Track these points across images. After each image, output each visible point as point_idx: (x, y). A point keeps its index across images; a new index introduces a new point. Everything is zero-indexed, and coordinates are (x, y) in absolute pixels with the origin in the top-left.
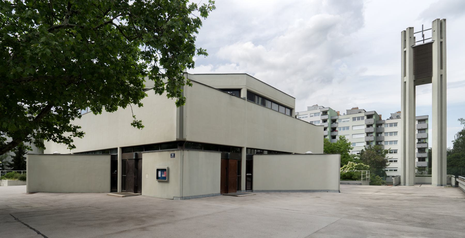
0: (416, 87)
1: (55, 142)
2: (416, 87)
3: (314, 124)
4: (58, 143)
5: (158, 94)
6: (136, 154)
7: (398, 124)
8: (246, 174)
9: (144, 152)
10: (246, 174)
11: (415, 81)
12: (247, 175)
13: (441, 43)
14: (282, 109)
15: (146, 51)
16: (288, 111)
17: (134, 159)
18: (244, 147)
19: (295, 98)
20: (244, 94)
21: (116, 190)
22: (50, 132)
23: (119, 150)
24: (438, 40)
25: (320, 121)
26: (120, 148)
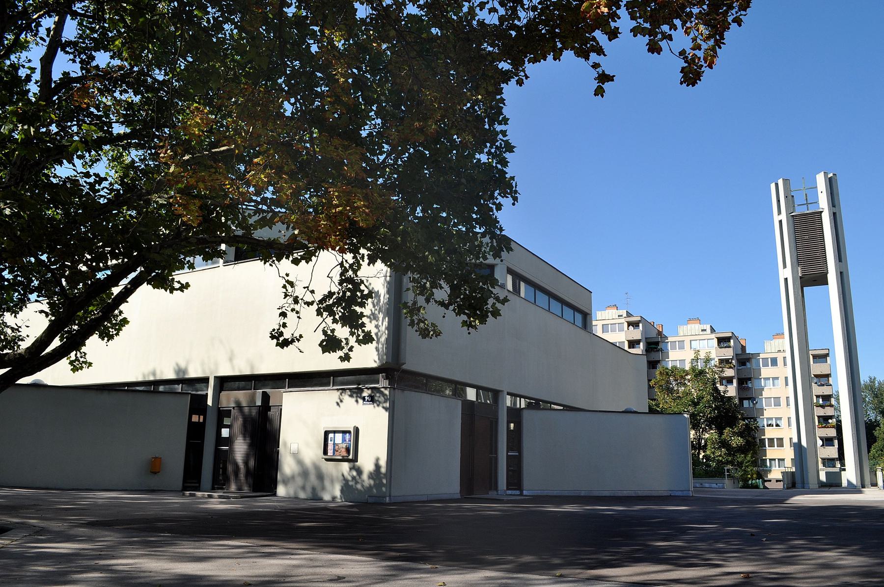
0: (805, 288)
1: (653, 53)
2: (805, 288)
3: (618, 345)
4: (282, 348)
5: (118, 336)
6: (264, 394)
7: (778, 359)
8: (507, 454)
9: (287, 390)
10: (507, 452)
11: (802, 278)
12: (509, 454)
13: (834, 214)
14: (568, 312)
15: (192, 257)
16: (579, 317)
17: (259, 406)
18: (502, 391)
19: (591, 292)
20: (298, 315)
21: (198, 485)
22: (68, 274)
23: (212, 382)
24: (830, 210)
25: (624, 342)
26: (215, 377)
